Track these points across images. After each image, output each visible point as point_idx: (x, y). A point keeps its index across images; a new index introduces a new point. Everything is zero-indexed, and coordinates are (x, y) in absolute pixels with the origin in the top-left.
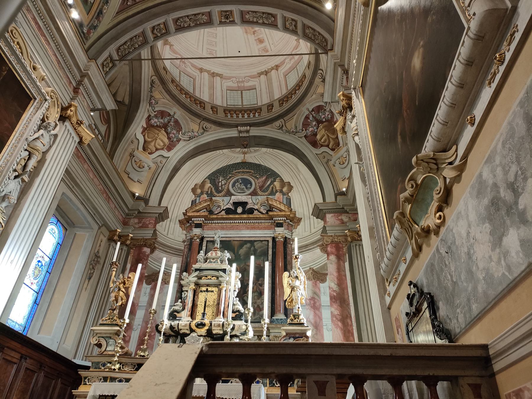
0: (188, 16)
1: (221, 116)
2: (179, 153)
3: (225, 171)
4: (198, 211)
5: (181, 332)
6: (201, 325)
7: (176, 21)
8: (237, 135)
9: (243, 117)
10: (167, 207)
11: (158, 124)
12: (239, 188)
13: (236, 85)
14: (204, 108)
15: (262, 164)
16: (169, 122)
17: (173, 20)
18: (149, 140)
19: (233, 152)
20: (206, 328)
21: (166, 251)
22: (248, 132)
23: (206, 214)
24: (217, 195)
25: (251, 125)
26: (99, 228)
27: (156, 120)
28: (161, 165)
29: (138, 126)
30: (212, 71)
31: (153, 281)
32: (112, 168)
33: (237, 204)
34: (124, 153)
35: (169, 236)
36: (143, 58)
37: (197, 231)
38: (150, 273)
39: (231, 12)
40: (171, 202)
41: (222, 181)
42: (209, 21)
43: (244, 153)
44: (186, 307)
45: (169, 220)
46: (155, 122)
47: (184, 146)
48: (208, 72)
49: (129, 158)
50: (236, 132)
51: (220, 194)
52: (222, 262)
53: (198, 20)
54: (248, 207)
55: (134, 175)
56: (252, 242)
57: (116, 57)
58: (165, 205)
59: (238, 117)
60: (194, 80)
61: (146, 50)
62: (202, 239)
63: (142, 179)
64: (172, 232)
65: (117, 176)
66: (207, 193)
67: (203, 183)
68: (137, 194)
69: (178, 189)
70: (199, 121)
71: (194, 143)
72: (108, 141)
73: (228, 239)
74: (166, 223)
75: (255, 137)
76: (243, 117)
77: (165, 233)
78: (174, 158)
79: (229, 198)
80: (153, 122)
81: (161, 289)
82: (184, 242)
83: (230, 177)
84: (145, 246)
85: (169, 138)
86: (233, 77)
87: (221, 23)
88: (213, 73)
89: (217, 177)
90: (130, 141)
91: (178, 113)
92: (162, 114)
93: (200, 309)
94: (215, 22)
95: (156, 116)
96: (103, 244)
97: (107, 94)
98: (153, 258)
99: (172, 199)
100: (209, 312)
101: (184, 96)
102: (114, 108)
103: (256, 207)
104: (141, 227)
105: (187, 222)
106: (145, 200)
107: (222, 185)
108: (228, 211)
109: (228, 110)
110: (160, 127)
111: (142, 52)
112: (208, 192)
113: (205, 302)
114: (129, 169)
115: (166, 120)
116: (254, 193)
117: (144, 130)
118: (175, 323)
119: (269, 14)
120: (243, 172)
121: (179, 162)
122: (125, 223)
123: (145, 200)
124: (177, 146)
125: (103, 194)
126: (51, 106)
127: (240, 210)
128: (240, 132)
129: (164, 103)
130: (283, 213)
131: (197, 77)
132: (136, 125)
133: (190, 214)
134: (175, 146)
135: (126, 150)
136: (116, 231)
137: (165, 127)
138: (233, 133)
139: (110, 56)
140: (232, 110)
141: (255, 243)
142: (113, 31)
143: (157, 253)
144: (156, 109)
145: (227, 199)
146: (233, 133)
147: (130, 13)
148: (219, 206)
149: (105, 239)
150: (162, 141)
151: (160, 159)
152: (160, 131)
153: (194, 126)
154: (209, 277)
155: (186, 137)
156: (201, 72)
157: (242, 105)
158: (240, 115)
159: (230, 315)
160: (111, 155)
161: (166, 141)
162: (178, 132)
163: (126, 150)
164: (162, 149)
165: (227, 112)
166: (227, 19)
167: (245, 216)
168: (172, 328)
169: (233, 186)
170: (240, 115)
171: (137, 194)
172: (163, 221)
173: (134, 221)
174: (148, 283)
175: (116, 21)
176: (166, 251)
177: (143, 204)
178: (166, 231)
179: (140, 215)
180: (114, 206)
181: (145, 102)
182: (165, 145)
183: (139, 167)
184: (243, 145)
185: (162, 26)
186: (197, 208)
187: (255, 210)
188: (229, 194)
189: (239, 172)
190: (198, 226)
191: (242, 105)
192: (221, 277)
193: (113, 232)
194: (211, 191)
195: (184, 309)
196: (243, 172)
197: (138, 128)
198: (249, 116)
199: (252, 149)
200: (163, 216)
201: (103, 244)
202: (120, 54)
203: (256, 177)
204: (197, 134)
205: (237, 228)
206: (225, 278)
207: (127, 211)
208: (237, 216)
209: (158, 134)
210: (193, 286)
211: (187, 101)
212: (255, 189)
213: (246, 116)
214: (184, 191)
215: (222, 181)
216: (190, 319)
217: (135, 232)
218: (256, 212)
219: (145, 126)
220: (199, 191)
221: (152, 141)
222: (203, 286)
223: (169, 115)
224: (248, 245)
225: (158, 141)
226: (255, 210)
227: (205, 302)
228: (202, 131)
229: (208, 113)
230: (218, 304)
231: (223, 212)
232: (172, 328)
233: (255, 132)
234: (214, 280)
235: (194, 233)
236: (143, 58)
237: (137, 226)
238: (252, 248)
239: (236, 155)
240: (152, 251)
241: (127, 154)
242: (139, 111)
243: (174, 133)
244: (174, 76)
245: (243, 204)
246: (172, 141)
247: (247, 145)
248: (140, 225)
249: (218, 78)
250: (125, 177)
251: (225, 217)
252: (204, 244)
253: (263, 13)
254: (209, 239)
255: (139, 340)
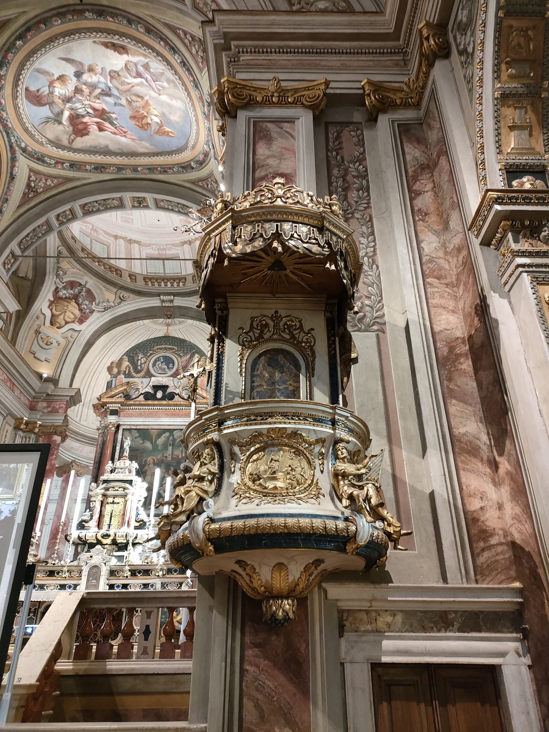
0: (96, 202)
1: (140, 285)
2: (92, 326)
3: (145, 347)
4: (112, 397)
5: (89, 541)
6: (106, 536)
7: (83, 207)
8: (159, 305)
9: (166, 285)
10: (79, 389)
11: (67, 295)
12: (160, 368)
13: (157, 252)
14: (121, 276)
15: (187, 339)
16: (80, 293)
17: (80, 206)
18: (57, 313)
19: (156, 323)
20: (111, 538)
21: (78, 440)
22: (171, 301)
23: (122, 400)
24: (136, 375)
25: (175, 295)
26: (4, 419)
27: (65, 292)
28: (72, 340)
29: (44, 300)
30: (129, 238)
31: (65, 473)
32: (16, 355)
33: (156, 388)
34: (29, 331)
35: (82, 422)
36: (48, 255)
37: (112, 419)
38: (62, 464)
39: (144, 198)
40: (84, 383)
41: (141, 359)
42: (120, 204)
43: (168, 325)
44: (94, 518)
45: (81, 404)
46: (64, 294)
47: (98, 318)
48: (124, 238)
49: (34, 335)
50: (159, 301)
51: (139, 375)
52: (130, 472)
53: (108, 204)
54: (169, 390)
55: (41, 354)
56: (171, 431)
57: (18, 252)
58: (77, 387)
59: (160, 285)
60: (108, 247)
61: (52, 236)
62: (118, 427)
63: (49, 357)
64: (85, 418)
65: (21, 363)
66: (124, 373)
67: (121, 360)
68: (45, 376)
69: (92, 367)
70: (115, 290)
71: (110, 314)
72: (10, 322)
73: (145, 427)
74: (79, 406)
75: (179, 307)
76: (166, 285)
77: (77, 419)
78: (87, 332)
79: (148, 379)
80: (61, 294)
81: (74, 481)
82: (98, 429)
83: (151, 354)
84: (56, 433)
85: (80, 310)
86: (153, 244)
87: (133, 207)
88: (130, 240)
89: (136, 354)
90: (35, 316)
91: (91, 282)
92: (72, 284)
93: (106, 519)
94: (127, 206)
95: (64, 288)
96: (8, 434)
97: (10, 298)
98: (64, 448)
99: (86, 379)
100: (115, 522)
101: (97, 264)
102: (18, 309)
103: (177, 391)
104: (51, 412)
105: (101, 408)
106: (53, 381)
107: (141, 364)
108: (148, 396)
109: (148, 278)
110: (69, 298)
111: (48, 238)
112: (125, 372)
113: (111, 514)
114: (35, 348)
115: (76, 291)
116: (175, 375)
117: (51, 303)
118: (83, 533)
119: (183, 205)
120: (166, 349)
121: (92, 336)
122: (32, 408)
123: (53, 381)
124: (90, 318)
125: (6, 383)
126: (65, 651)
127: (159, 394)
128: (163, 301)
129: (72, 271)
130: (205, 401)
131: (112, 244)
132: (41, 300)
133: (105, 401)
134: (87, 318)
135: (30, 327)
136: (23, 418)
137: (76, 298)
138: (155, 302)
139: (12, 253)
140: (154, 278)
141: (175, 432)
142: (14, 226)
143: (68, 441)
144: (65, 280)
145: (146, 380)
146: (155, 302)
147: (32, 204)
148: (137, 389)
149: (10, 429)
150: (72, 313)
151: (71, 332)
152: (70, 303)
153: (110, 295)
154: (116, 488)
155: (100, 308)
156: (116, 239)
157: (165, 273)
158: (163, 283)
159: (133, 524)
160: (13, 342)
161: (77, 313)
162: (91, 302)
163: (30, 327)
164: (73, 322)
165: (147, 280)
166: (140, 204)
167: (164, 402)
168: (79, 538)
169: (154, 364)
170: (163, 283)
171: (45, 376)
172: (75, 405)
173: (42, 405)
174: (59, 475)
175: (17, 215)
176: (78, 440)
177: (52, 387)
178: (79, 417)
179: (49, 398)
180: (19, 392)
181: (51, 274)
182: (76, 317)
183: (47, 344)
184: (167, 315)
185: (68, 212)
186: (113, 393)
187: (177, 394)
188: (149, 375)
189: (161, 349)
190: (115, 412)
191: (165, 273)
192: (127, 489)
193: (19, 420)
194: (129, 371)
195: (91, 519)
196: (166, 349)
197: (44, 303)
198: (172, 285)
199: (176, 320)
200: (75, 399)
201: (8, 434)
202: (22, 247)
203: (179, 355)
204: (113, 305)
205: (156, 415)
206: (131, 489)
207: (34, 394)
208: (156, 402)
209: (67, 307)
210: (100, 498)
211: (101, 269)
212: (177, 370)
213: (169, 285)
214: (99, 370)
215: (141, 359)
216: (96, 529)
217: (44, 418)
218: (177, 397)
219: (52, 299)
220: (115, 370)
221: (61, 314)
222: (110, 496)
223: (80, 285)
224: (167, 434)
225: (68, 313)
226: (177, 394)
227: (111, 514)
228: (119, 300)
229: (126, 281)
230: (124, 514)
231: (142, 396)
232: (79, 538)
233: (179, 302)
234: (121, 492)
235: (109, 421)
236: (48, 255)
237: (45, 411)
238: (171, 438)
239: (159, 327)
240: (63, 440)
241: (32, 331)
242: (45, 284)
243: (86, 304)
244: (85, 244)
245: (164, 388)
246: (85, 313)
247: (171, 315)
248: (49, 409)
249: (136, 245)
250: (30, 359)
251: (143, 403)
252: (120, 432)
253: (178, 204)
254: (125, 427)
255: (51, 534)
